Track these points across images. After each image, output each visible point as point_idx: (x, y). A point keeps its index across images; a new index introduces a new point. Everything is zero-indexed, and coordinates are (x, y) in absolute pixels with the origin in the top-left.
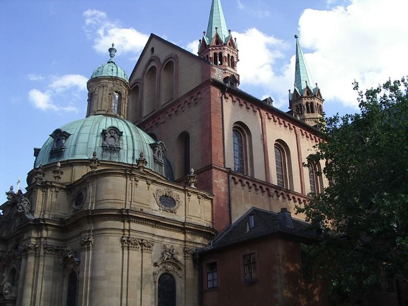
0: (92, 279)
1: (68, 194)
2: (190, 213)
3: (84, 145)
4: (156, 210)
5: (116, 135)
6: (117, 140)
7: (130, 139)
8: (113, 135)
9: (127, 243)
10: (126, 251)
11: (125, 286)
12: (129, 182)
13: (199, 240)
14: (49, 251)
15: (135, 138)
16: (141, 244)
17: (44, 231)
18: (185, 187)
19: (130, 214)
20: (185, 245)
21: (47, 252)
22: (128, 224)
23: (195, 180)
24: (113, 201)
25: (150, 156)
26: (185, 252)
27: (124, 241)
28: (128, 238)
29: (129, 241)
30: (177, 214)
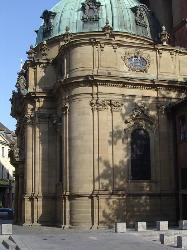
0: (70, 139)
1: (55, 68)
2: (162, 70)
3: (67, 20)
4: (125, 72)
5: (94, 7)
6: (96, 10)
7: (109, 7)
8: (91, 6)
9: (96, 105)
10: (95, 113)
11: (96, 143)
12: (95, 49)
13: (173, 94)
14: (42, 119)
15: (114, 5)
16: (111, 105)
17: (37, 102)
18: (154, 47)
19: (95, 79)
20: (158, 102)
21: (41, 120)
22: (97, 88)
23: (166, 37)
24: (82, 69)
25: (131, 20)
26: (158, 107)
27: (93, 103)
28: (97, 100)
29: (97, 103)
30: (148, 72)
